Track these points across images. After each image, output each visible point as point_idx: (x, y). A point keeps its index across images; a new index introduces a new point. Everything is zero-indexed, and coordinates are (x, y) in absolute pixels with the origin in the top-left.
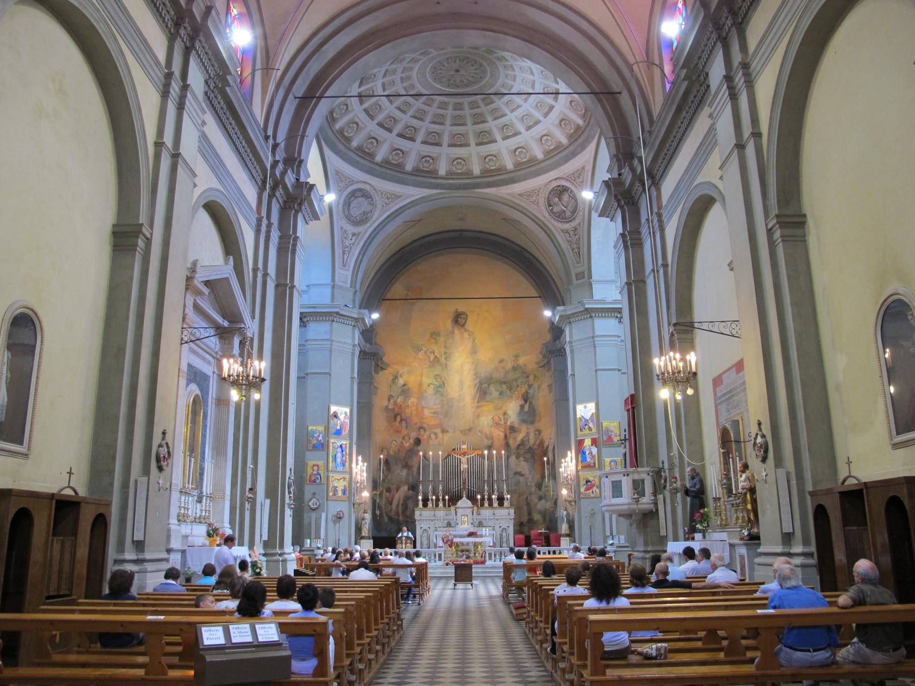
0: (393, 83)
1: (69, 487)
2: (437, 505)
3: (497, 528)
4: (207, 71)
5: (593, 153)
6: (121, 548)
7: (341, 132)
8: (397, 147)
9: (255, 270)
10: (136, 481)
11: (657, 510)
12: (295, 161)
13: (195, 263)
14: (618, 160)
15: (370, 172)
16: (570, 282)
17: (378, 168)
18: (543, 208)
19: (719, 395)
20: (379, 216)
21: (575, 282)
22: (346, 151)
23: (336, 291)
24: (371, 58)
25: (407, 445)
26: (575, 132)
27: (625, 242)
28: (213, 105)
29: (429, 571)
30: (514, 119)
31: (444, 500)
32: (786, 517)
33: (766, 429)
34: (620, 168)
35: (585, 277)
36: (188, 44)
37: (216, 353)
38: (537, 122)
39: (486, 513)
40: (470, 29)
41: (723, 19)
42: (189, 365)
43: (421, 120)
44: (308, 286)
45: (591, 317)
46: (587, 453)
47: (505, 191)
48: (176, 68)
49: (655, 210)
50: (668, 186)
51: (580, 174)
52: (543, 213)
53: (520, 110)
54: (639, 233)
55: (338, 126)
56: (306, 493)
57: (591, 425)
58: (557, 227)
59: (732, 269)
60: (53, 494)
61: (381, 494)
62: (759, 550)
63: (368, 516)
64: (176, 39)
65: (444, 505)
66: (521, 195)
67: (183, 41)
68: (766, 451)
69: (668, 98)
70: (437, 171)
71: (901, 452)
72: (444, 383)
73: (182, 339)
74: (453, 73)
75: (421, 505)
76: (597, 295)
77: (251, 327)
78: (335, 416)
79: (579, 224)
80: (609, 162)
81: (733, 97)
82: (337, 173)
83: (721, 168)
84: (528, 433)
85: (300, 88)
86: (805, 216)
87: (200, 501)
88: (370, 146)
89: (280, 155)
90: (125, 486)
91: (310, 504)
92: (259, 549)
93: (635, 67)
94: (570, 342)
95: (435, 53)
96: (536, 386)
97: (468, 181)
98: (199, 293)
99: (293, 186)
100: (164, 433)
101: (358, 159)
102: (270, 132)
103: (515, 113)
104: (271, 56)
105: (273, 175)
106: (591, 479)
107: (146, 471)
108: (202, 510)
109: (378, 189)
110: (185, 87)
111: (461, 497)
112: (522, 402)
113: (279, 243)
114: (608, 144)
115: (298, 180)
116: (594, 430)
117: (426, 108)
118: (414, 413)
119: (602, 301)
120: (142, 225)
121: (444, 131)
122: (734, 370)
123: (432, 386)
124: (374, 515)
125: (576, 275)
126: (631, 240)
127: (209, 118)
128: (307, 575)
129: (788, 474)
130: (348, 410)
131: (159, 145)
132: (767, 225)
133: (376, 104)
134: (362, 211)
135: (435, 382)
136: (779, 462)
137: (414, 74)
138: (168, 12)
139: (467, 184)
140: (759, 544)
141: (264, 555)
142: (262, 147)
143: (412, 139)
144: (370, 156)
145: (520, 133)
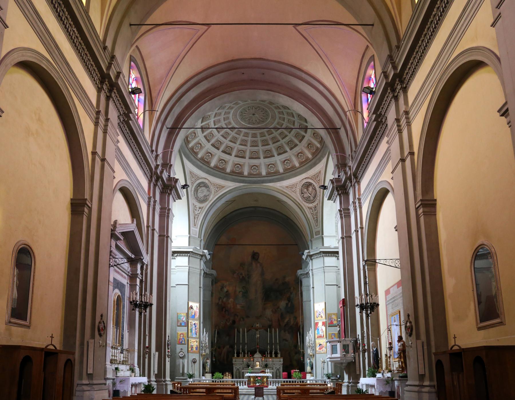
0: (219, 121)
1: (52, 344)
2: (244, 356)
3: (274, 368)
4: (119, 111)
6: (81, 378)
7: (192, 149)
8: (222, 158)
9: (148, 227)
10: (88, 342)
11: (355, 361)
12: (167, 165)
13: (115, 222)
14: (338, 168)
15: (208, 172)
16: (312, 236)
18: (299, 195)
19: (388, 300)
20: (213, 198)
21: (315, 237)
23: (191, 239)
24: (207, 105)
25: (228, 324)
27: (341, 214)
28: (123, 131)
31: (248, 353)
32: (421, 366)
33: (412, 319)
34: (339, 173)
35: (321, 233)
36: (108, 94)
38: (296, 145)
40: (260, 89)
41: (396, 85)
42: (114, 279)
43: (235, 143)
45: (323, 256)
46: (320, 329)
47: (278, 185)
48: (102, 108)
49: (357, 197)
50: (364, 182)
51: (318, 176)
52: (297, 196)
53: (287, 138)
54: (349, 209)
55: (190, 145)
57: (322, 315)
58: (306, 205)
59: (396, 230)
60: (43, 348)
62: (407, 383)
63: (209, 361)
65: (248, 356)
66: (287, 187)
67: (105, 92)
68: (412, 331)
69: (364, 132)
70: (243, 173)
71: (482, 332)
73: (110, 264)
74: (251, 115)
75: (236, 356)
77: (146, 259)
78: (192, 308)
80: (333, 169)
81: (400, 131)
82: (191, 172)
83: (392, 173)
85: (170, 123)
86: (436, 200)
87: (122, 353)
89: (160, 162)
90: (82, 344)
92: (153, 378)
93: (348, 113)
94: (312, 270)
95: (241, 103)
98: (117, 239)
99: (167, 179)
100: (102, 316)
101: (201, 165)
102: (154, 148)
103: (284, 140)
104: (154, 103)
105: (156, 173)
106: (322, 343)
107: (93, 337)
110: (107, 120)
111: (256, 352)
112: (287, 302)
113: (160, 212)
114: (333, 159)
115: (169, 176)
116: (324, 317)
117: (237, 136)
120: (86, 199)
121: (246, 150)
122: (396, 286)
126: (344, 213)
127: (121, 138)
128: (177, 393)
129: (423, 343)
130: (198, 305)
131: (94, 153)
132: (415, 205)
133: (211, 133)
135: (243, 291)
136: (418, 337)
137: (231, 115)
138: (97, 75)
140: (407, 380)
141: (156, 381)
142: (150, 157)
143: (230, 154)
144: (208, 163)
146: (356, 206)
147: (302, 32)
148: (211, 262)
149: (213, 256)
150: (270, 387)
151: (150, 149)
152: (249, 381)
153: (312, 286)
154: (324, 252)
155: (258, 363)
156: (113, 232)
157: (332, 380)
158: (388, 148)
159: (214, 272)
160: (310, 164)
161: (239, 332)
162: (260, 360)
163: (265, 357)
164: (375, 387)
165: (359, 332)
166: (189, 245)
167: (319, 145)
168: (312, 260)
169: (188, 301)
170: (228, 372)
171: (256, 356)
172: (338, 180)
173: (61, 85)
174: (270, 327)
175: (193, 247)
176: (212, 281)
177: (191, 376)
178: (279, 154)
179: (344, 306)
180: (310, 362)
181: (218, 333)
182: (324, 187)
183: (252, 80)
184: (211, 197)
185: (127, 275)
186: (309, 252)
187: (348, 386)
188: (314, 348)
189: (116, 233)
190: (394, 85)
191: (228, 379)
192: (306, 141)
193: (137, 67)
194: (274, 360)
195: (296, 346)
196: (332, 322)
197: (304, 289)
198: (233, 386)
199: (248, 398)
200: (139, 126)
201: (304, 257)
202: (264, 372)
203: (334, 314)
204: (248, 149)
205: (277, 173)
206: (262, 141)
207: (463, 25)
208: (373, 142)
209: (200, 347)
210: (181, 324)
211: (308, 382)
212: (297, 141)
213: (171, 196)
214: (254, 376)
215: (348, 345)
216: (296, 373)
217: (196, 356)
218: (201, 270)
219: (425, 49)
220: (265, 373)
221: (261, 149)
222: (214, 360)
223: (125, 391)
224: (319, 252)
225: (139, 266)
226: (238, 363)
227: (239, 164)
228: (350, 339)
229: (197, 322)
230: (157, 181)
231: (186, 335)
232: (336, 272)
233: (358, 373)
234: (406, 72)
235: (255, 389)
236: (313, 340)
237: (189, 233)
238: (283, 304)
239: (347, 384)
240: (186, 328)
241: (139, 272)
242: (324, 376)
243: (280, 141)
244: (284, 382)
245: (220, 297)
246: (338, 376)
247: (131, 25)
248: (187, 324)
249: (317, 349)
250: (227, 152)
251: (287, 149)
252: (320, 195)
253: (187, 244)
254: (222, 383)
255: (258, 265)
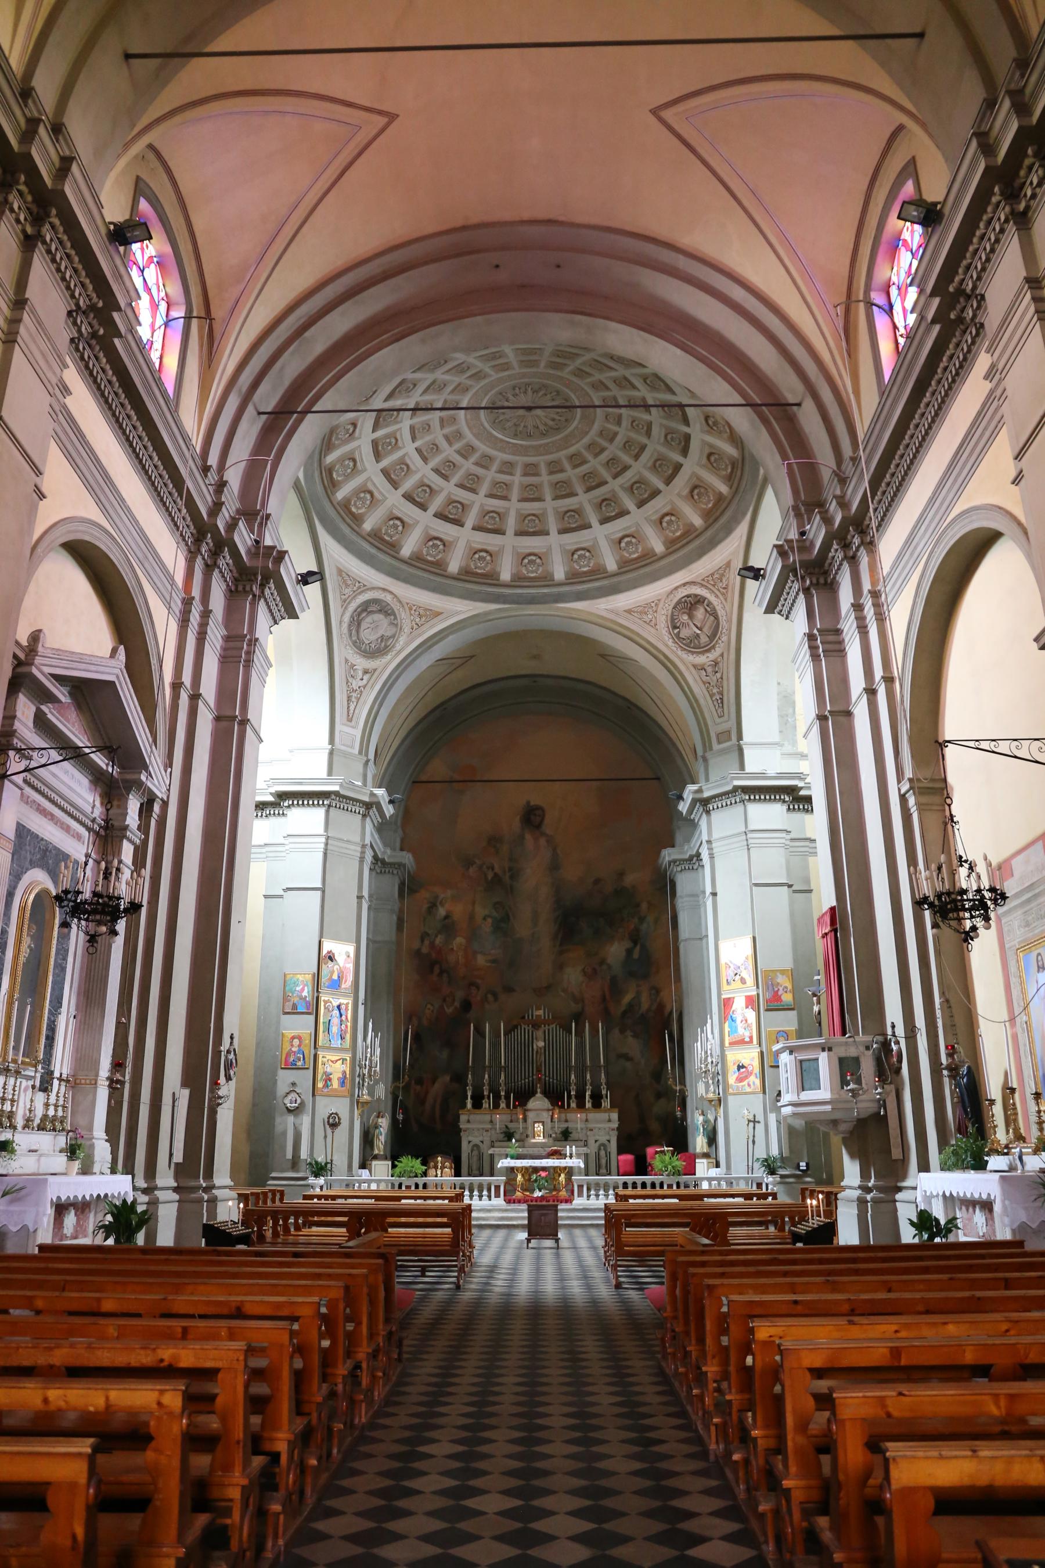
2: (496, 1106)
3: (591, 1142)
5: (744, 538)
7: (346, 505)
9: (177, 686)
12: (253, 514)
13: (35, 637)
14: (798, 515)
16: (707, 746)
17: (404, 567)
18: (664, 632)
20: (407, 644)
21: (716, 747)
22: (354, 537)
23: (335, 758)
25: (449, 1011)
26: (715, 505)
27: (813, 648)
29: (474, 1215)
30: (617, 489)
31: (507, 1098)
34: (801, 525)
36: (29, 230)
37: (94, 820)
38: (656, 493)
39: (577, 1120)
43: (473, 491)
44: (291, 751)
46: (738, 1021)
49: (867, 586)
50: (890, 543)
51: (723, 575)
52: (661, 637)
53: (629, 474)
54: (838, 632)
55: (340, 495)
56: (279, 1083)
57: (745, 974)
58: (685, 660)
61: (407, 1088)
63: (384, 1123)
64: (35, 246)
67: (18, 221)
69: (884, 392)
72: (508, 915)
75: (469, 1105)
76: (750, 767)
77: (160, 780)
78: (331, 958)
79: (722, 655)
82: (340, 572)
84: (638, 994)
85: (268, 397)
87: (45, 1087)
88: (391, 531)
91: (287, 1101)
92: (165, 1178)
94: (709, 842)
95: (494, 376)
96: (650, 919)
97: (545, 590)
98: (43, 695)
99: (249, 552)
101: (373, 551)
102: (213, 460)
103: (620, 480)
104: (217, 335)
106: (745, 1062)
108: (47, 1105)
109: (404, 601)
111: (533, 1094)
113: (224, 649)
116: (750, 981)
117: (480, 471)
118: (461, 960)
119: (762, 776)
123: (489, 920)
124: (394, 1121)
125: (717, 736)
126: (825, 644)
127: (73, 376)
130: (351, 949)
132: (899, 790)
134: (379, 635)
135: (495, 914)
139: (545, 594)
141: (176, 1190)
143: (459, 523)
144: (392, 547)
145: (628, 513)
146: (864, 618)
147: (676, 127)
148: (400, 831)
149: (407, 814)
150: (578, 1202)
151: (199, 463)
152: (510, 1183)
153: (709, 890)
154: (745, 790)
155: (539, 1128)
156: (22, 670)
157: (782, 1177)
158: (992, 392)
159: (407, 858)
160: (697, 543)
161: (480, 1032)
162: (546, 1116)
163: (562, 1106)
164: (997, 1208)
165: (893, 1012)
166: (330, 772)
167: (724, 489)
168: (708, 812)
169: (321, 936)
170: (445, 1154)
171: (532, 1104)
172: (803, 543)
173: (127, 574)
174: (578, 1017)
175: (339, 778)
176: (402, 885)
177: (319, 1170)
178: (604, 521)
179: (835, 931)
180: (706, 1122)
181: (417, 1037)
182: (757, 574)
183: (523, 286)
184: (402, 640)
185: (89, 829)
186: (700, 791)
187: (862, 1202)
188: (719, 1077)
189: (35, 671)
190: (1016, 174)
191: (442, 1177)
192: (687, 477)
193: (161, 220)
194: (592, 1116)
195: (658, 1074)
196: (776, 997)
197: (682, 903)
198: (456, 1205)
199: (506, 1239)
200: (149, 362)
201: (683, 807)
202: (558, 1154)
203: (783, 972)
204: (513, 509)
205: (598, 572)
206: (556, 485)
207: (944, 499)
208: (925, 400)
209: (355, 1079)
210: (295, 1006)
211: (705, 1186)
212: (657, 482)
213: (262, 608)
214: (527, 1168)
215: (856, 1060)
216: (661, 1157)
217: (341, 1107)
218: (364, 846)
219: (961, 367)
220: (565, 1157)
221: (550, 507)
222: (400, 1117)
223: (25, 1227)
224: (729, 788)
225: (133, 805)
226: (476, 1127)
227: (486, 551)
228: (861, 1037)
229: (347, 1001)
230: (216, 553)
231: (308, 1041)
232: (786, 847)
233: (896, 1153)
234: (942, 365)
235: (530, 1212)
236: (717, 1051)
237: (332, 741)
238: (615, 951)
239: (859, 1192)
240: (312, 1018)
241: (132, 819)
242: (757, 1165)
243: (606, 483)
244: (625, 1185)
245: (428, 935)
246: (803, 1165)
247: (128, 56)
248: (314, 1008)
249: (732, 1079)
250: (452, 515)
251: (629, 504)
252: (729, 630)
253: (323, 773)
254: (421, 1193)
255: (542, 841)
